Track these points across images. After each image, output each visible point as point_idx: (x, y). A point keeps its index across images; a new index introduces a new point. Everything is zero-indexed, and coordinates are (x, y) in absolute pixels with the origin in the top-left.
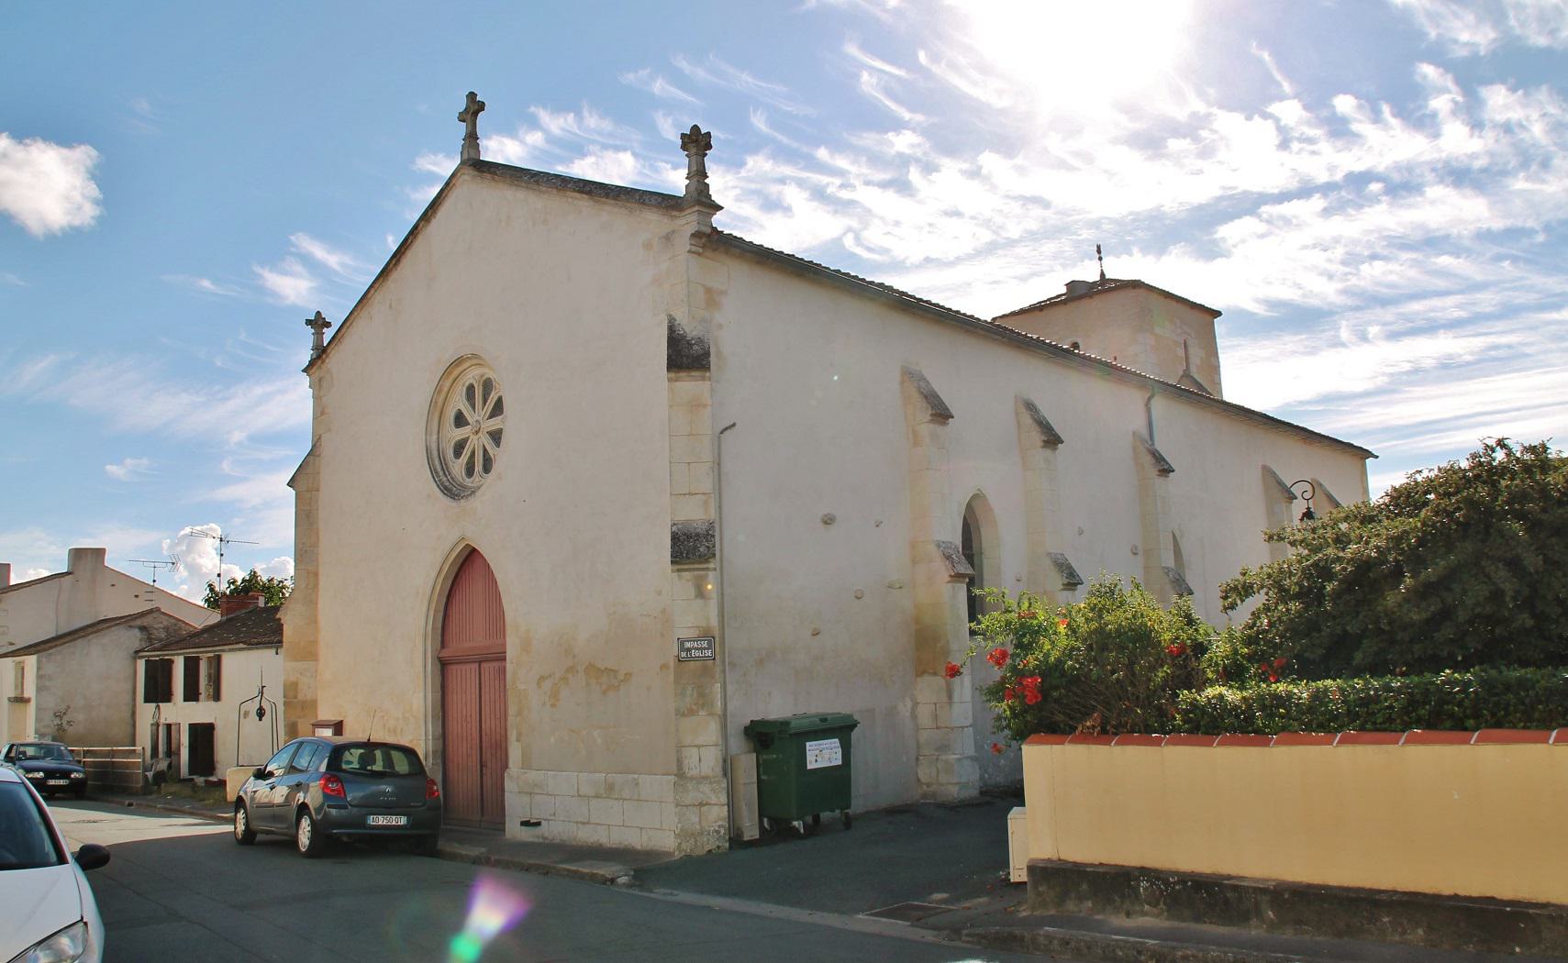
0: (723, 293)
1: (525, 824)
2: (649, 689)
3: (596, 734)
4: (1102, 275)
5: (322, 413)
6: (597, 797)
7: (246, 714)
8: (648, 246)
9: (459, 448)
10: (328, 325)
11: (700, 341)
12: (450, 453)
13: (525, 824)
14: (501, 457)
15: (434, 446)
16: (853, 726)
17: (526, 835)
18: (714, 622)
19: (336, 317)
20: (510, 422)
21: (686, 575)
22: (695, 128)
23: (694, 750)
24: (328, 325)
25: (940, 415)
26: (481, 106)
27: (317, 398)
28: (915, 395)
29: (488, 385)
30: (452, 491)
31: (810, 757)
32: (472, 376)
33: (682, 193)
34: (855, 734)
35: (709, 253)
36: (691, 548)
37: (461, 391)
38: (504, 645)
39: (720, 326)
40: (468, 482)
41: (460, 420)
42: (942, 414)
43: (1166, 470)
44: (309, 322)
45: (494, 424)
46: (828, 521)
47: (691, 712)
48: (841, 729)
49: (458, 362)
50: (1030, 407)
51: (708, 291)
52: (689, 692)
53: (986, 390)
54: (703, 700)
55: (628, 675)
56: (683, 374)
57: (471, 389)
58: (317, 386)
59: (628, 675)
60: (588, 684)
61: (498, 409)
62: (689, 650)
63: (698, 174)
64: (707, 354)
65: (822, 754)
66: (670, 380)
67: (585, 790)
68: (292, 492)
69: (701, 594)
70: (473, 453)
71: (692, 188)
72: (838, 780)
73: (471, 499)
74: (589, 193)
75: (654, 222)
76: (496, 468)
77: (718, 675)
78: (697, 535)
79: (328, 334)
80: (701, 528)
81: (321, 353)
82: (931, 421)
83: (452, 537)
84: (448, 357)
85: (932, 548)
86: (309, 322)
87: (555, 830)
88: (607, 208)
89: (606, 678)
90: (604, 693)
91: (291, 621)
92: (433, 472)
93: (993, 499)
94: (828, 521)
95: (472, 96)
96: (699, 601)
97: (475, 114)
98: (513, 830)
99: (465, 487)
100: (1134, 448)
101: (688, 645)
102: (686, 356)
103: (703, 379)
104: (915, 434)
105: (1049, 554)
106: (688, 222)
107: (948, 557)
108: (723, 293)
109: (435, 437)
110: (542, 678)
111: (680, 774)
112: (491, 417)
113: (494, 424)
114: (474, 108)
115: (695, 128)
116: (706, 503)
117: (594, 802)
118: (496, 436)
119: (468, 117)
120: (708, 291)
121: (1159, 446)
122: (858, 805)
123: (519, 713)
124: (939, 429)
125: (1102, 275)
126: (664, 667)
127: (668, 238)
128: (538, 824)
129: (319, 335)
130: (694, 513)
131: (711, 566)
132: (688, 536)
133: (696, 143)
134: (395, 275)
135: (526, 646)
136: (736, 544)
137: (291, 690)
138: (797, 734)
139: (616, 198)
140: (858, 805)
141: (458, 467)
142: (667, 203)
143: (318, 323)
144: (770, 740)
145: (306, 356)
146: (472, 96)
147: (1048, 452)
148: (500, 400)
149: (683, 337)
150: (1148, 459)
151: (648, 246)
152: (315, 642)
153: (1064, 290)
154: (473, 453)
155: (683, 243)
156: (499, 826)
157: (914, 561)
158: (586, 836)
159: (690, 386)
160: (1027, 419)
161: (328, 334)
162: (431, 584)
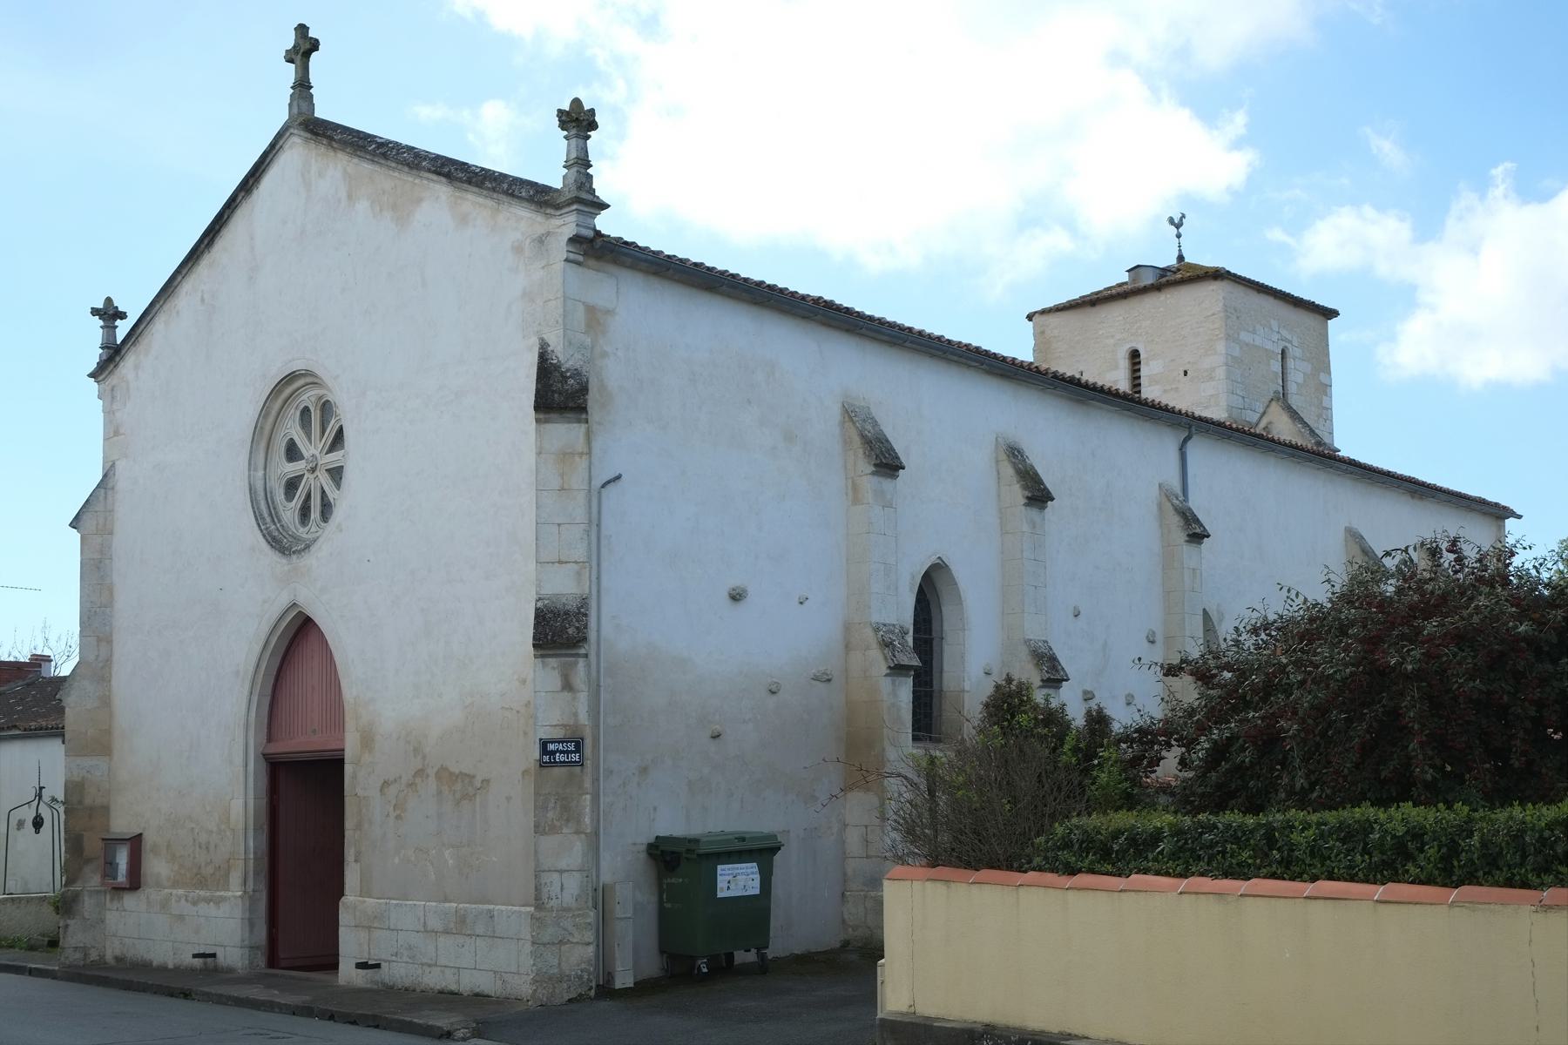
0: (609, 312)
1: (362, 966)
2: (508, 799)
3: (447, 853)
4: (1181, 258)
5: (116, 433)
6: (447, 932)
7: (21, 824)
8: (518, 249)
9: (292, 485)
10: (123, 316)
11: (577, 373)
12: (280, 495)
13: (362, 966)
14: (346, 501)
15: (259, 485)
16: (775, 849)
17: (359, 978)
18: (584, 718)
19: (134, 309)
20: (353, 456)
21: (553, 662)
22: (576, 102)
23: (556, 876)
24: (123, 316)
25: (887, 466)
26: (314, 45)
27: (109, 413)
28: (857, 440)
29: (326, 408)
30: (281, 543)
31: (722, 882)
32: (308, 398)
33: (558, 184)
34: (777, 858)
35: (592, 262)
36: (559, 631)
37: (293, 415)
38: (343, 740)
39: (604, 355)
40: (302, 532)
41: (292, 453)
42: (888, 464)
43: (1197, 536)
44: (95, 312)
45: (334, 458)
46: (736, 597)
47: (553, 830)
48: (762, 852)
49: (291, 378)
50: (1014, 454)
51: (591, 310)
52: (551, 805)
53: (951, 432)
54: (568, 813)
55: (486, 782)
56: (553, 416)
57: (306, 412)
58: (110, 398)
59: (486, 782)
60: (440, 793)
61: (338, 440)
62: (553, 753)
63: (580, 163)
64: (584, 389)
65: (738, 880)
66: (537, 421)
67: (435, 923)
68: (75, 536)
69: (567, 686)
70: (308, 496)
71: (571, 180)
72: (754, 913)
73: (305, 555)
74: (448, 176)
75: (522, 220)
76: (338, 514)
77: (588, 784)
78: (567, 613)
79: (123, 328)
80: (572, 605)
81: (113, 354)
82: (873, 473)
83: (283, 601)
84: (277, 372)
85: (869, 632)
86: (95, 312)
87: (398, 972)
88: (470, 196)
89: (461, 786)
90: (458, 803)
91: (75, 705)
92: (258, 517)
93: (960, 571)
94: (736, 597)
95: (302, 30)
96: (567, 695)
97: (307, 55)
98: (347, 972)
99: (297, 539)
100: (1160, 506)
101: (551, 747)
102: (560, 394)
103: (579, 421)
104: (855, 489)
105: (1027, 642)
106: (567, 225)
107: (886, 644)
108: (609, 312)
109: (261, 473)
110: (386, 784)
111: (539, 904)
112: (330, 450)
113: (334, 458)
114: (304, 48)
115: (576, 102)
116: (579, 574)
117: (442, 939)
118: (336, 474)
119: (298, 58)
120: (591, 310)
121: (1196, 503)
122: (778, 947)
123: (359, 826)
124: (887, 484)
125: (1181, 258)
126: (525, 772)
127: (541, 241)
128: (377, 966)
129: (110, 328)
130: (564, 586)
131: (582, 651)
132: (556, 614)
133: (578, 121)
134: (206, 261)
135: (367, 741)
136: (618, 627)
137: (74, 789)
138: (708, 856)
139: (480, 185)
140: (778, 947)
141: (289, 512)
142: (538, 196)
143: (109, 314)
144: (673, 860)
145: (94, 356)
146: (302, 30)
147: (1033, 513)
148: (340, 431)
149: (557, 367)
150: (1175, 521)
151: (518, 249)
152: (108, 732)
153: (1125, 278)
154: (308, 496)
155: (559, 248)
156: (333, 965)
157: (847, 647)
158: (434, 979)
159: (565, 432)
160: (1008, 471)
161: (123, 328)
162: (254, 660)
